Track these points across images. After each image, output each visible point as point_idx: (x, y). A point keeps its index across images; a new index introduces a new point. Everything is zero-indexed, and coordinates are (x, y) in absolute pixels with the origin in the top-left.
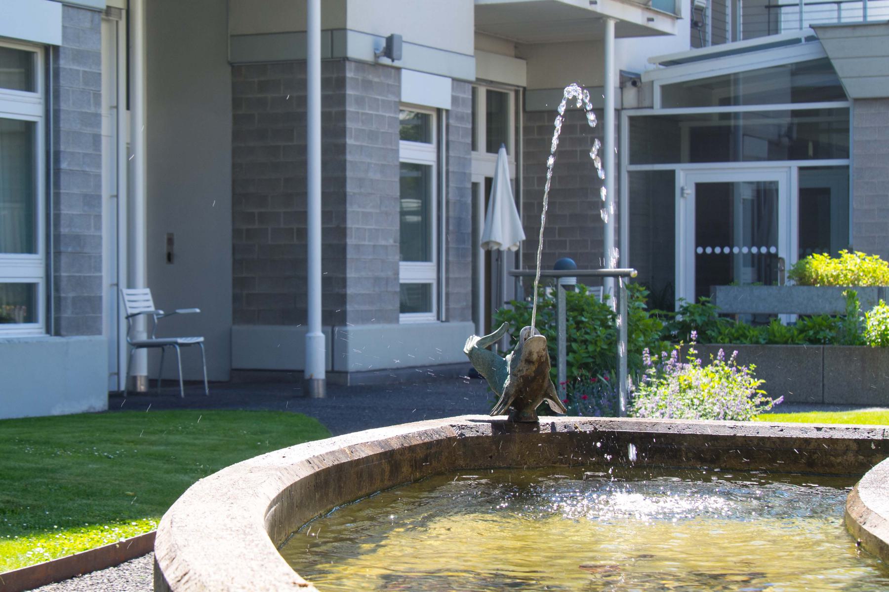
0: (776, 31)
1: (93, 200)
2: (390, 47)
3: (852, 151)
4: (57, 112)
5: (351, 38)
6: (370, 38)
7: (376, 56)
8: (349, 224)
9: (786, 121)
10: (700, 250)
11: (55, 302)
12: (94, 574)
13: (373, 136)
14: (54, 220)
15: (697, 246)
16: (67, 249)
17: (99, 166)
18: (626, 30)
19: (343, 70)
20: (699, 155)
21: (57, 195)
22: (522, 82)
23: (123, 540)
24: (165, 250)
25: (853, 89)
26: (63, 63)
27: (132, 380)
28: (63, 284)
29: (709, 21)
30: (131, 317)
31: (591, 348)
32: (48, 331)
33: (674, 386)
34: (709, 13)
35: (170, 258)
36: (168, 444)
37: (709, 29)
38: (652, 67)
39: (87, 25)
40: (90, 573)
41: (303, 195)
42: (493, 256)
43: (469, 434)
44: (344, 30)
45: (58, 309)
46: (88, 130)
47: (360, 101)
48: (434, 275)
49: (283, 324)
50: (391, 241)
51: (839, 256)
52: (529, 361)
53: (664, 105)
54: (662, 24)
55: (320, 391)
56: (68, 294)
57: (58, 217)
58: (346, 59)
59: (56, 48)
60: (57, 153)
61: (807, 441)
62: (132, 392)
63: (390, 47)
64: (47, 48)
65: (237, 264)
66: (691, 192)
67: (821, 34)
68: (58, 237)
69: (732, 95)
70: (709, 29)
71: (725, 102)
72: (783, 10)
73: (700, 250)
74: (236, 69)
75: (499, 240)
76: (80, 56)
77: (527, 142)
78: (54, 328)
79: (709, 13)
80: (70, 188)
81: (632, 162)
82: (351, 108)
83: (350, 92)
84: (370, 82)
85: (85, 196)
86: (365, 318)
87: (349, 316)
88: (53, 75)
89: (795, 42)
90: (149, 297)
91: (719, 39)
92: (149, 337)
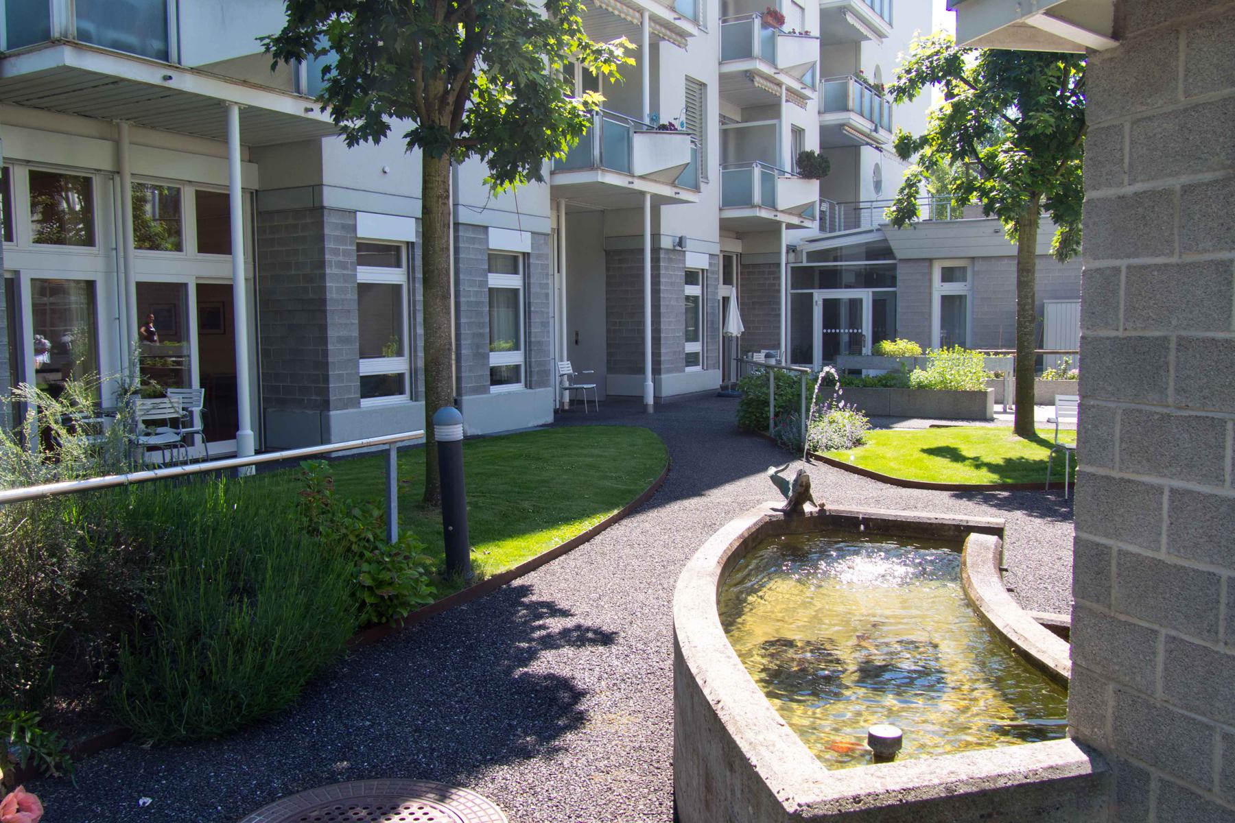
0: (859, 227)
1: (545, 324)
2: (681, 242)
3: (898, 283)
4: (529, 283)
5: (663, 238)
6: (671, 238)
7: (674, 246)
8: (662, 327)
9: (863, 267)
10: (825, 331)
11: (529, 373)
12: (580, 547)
13: (672, 284)
14: (528, 334)
15: (824, 328)
16: (534, 348)
17: (548, 308)
18: (790, 226)
19: (659, 253)
20: (823, 286)
21: (530, 323)
22: (740, 250)
23: (591, 528)
24: (574, 339)
25: (899, 254)
26: (531, 261)
27: (562, 403)
28: (533, 364)
29: (828, 218)
30: (562, 375)
31: (784, 398)
32: (526, 387)
33: (826, 420)
34: (828, 213)
35: (577, 342)
36: (592, 456)
37: (828, 222)
38: (802, 243)
39: (542, 241)
40: (578, 547)
41: (643, 313)
42: (727, 339)
43: (774, 519)
44: (660, 234)
45: (531, 376)
46: (543, 291)
47: (667, 268)
48: (701, 348)
49: (630, 374)
50: (681, 334)
51: (895, 341)
52: (801, 486)
53: (808, 262)
54: (807, 223)
55: (651, 410)
56: (535, 369)
57: (530, 333)
58: (660, 248)
59: (528, 254)
60: (529, 303)
61: (931, 524)
62: (563, 410)
63: (681, 242)
64: (524, 254)
65: (609, 345)
66: (820, 303)
67: (883, 228)
68: (530, 342)
69: (839, 254)
70: (828, 222)
71: (836, 260)
72: (862, 211)
73: (825, 331)
74: (608, 253)
75: (731, 331)
76: (539, 257)
77: (742, 279)
78: (529, 385)
79: (828, 213)
80: (535, 319)
81: (792, 289)
82: (662, 272)
83: (662, 264)
84: (671, 258)
85: (542, 322)
86: (669, 371)
87: (662, 371)
88: (527, 266)
89: (871, 231)
90: (570, 365)
91: (832, 230)
92: (570, 385)
